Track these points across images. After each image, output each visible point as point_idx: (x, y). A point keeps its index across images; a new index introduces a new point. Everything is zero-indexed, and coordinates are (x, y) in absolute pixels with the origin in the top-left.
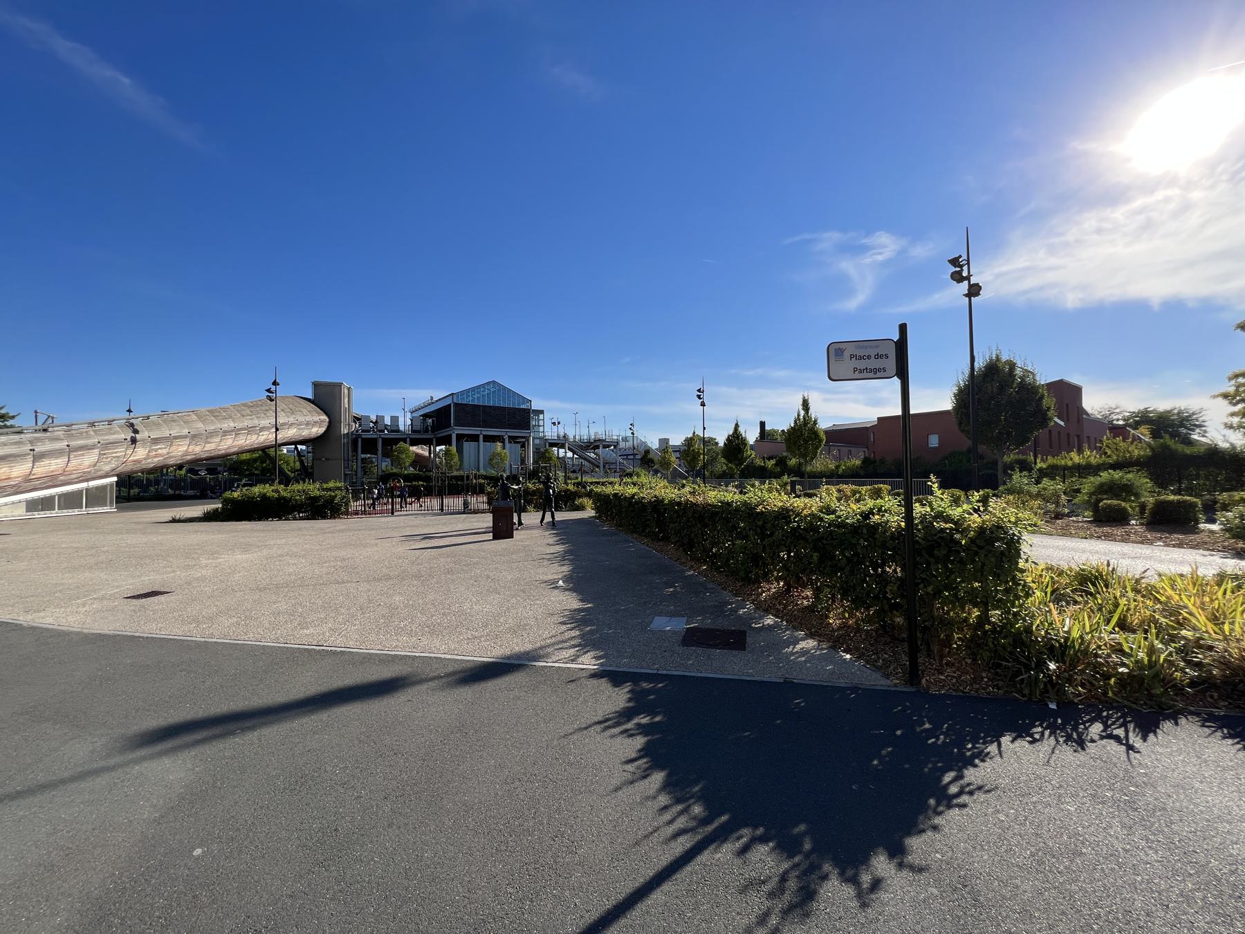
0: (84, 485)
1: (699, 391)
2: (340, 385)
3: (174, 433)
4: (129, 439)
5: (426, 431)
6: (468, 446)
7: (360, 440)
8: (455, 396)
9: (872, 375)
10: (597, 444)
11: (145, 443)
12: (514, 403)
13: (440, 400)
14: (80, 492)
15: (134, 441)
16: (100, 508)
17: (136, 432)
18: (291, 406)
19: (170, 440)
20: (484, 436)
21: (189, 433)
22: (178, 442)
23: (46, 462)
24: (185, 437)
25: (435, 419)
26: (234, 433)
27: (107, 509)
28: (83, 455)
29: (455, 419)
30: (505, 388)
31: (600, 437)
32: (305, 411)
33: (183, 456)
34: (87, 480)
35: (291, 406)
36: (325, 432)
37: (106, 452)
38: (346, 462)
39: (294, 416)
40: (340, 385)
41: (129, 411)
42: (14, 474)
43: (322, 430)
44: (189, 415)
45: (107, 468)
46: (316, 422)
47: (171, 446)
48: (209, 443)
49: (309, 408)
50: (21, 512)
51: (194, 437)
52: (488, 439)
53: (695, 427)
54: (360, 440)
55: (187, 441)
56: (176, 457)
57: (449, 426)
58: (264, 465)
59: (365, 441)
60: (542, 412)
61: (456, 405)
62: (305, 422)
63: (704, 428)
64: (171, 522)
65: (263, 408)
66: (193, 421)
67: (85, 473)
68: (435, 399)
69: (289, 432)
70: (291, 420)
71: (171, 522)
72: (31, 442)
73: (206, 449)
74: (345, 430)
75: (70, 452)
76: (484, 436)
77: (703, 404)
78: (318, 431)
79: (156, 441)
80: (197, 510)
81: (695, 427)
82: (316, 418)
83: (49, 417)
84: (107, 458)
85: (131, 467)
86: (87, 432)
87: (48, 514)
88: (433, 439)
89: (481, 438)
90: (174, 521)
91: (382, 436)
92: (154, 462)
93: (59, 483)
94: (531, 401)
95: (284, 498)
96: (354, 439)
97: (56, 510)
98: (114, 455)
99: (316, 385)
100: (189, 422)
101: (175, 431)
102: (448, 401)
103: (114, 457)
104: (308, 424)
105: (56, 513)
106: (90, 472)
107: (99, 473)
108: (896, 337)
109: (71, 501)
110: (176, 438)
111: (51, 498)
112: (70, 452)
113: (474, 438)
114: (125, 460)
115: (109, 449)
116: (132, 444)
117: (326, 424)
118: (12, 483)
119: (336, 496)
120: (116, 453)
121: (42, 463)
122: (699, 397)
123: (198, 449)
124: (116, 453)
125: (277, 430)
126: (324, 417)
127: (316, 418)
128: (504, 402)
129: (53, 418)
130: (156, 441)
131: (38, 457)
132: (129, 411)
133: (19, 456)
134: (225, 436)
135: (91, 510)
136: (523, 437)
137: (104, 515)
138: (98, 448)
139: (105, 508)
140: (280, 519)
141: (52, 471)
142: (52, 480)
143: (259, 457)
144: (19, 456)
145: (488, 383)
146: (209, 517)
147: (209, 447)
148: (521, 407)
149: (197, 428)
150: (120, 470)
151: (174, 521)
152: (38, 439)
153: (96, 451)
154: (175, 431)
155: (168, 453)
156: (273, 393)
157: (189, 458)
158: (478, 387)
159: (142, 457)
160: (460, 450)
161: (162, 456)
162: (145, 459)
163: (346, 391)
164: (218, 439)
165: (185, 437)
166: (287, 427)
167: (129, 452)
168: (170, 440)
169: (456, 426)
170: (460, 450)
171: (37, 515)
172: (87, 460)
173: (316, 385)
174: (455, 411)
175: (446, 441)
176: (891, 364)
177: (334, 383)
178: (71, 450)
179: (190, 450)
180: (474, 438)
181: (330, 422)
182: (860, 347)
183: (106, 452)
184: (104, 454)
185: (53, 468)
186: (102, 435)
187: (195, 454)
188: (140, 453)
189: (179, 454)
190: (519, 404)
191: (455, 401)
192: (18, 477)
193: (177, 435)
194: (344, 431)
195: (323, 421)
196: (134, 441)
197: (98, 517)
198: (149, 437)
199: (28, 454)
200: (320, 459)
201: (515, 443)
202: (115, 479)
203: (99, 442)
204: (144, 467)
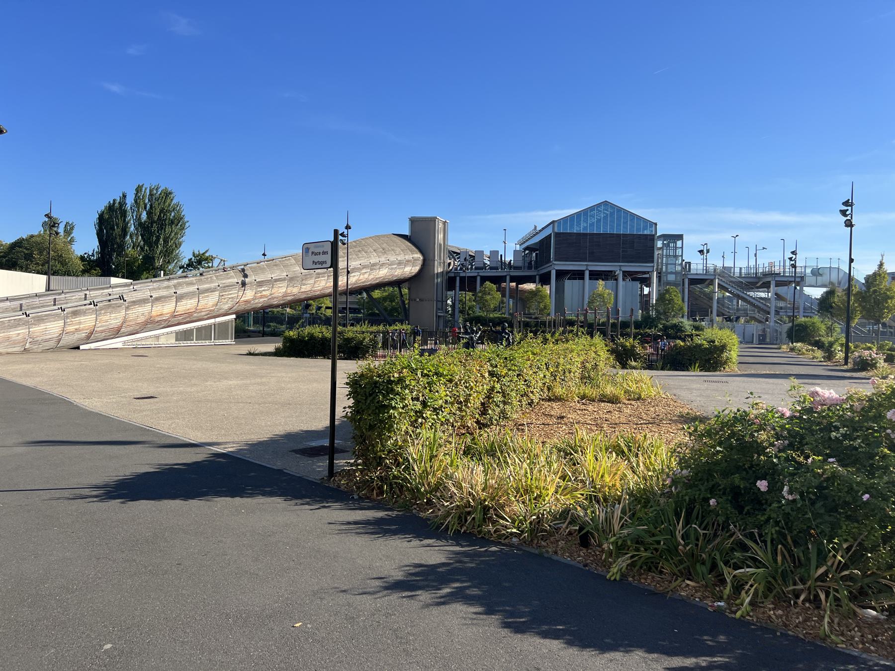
0: (212, 321)
1: (846, 203)
2: (433, 220)
3: (275, 276)
4: (240, 283)
5: (530, 267)
6: (570, 285)
7: (458, 279)
8: (556, 224)
9: (320, 266)
10: (768, 279)
11: (252, 286)
12: (638, 229)
13: (543, 229)
14: (210, 326)
15: (244, 284)
16: (224, 341)
17: (246, 276)
18: (385, 245)
19: (272, 282)
20: (590, 271)
21: (287, 276)
22: (279, 284)
23: (184, 302)
24: (284, 280)
25: (538, 252)
26: (326, 275)
27: (228, 342)
28: (208, 296)
29: (555, 253)
30: (620, 209)
31: (777, 270)
32: (398, 250)
33: (283, 296)
34: (215, 317)
35: (385, 245)
36: (420, 271)
37: (224, 293)
38: (440, 304)
39: (385, 256)
40: (433, 220)
41: (264, 255)
42: (165, 311)
43: (416, 269)
44: (289, 259)
45: (226, 307)
46: (408, 261)
47: (272, 287)
48: (305, 284)
49: (403, 247)
50: (172, 341)
51: (291, 280)
52: (596, 275)
53: (882, 256)
54: (458, 279)
55: (285, 284)
56: (277, 298)
57: (549, 261)
58: (394, 304)
59: (462, 279)
60: (680, 237)
61: (558, 235)
62: (397, 262)
63: (851, 261)
64: (247, 354)
65: (356, 250)
66: (291, 265)
67: (211, 311)
68: (539, 228)
69: (381, 272)
70: (383, 259)
71: (247, 354)
72: (175, 286)
73: (302, 290)
74: (439, 269)
75: (199, 294)
76: (590, 271)
77: (849, 224)
78: (411, 270)
79: (260, 284)
80: (271, 348)
81: (882, 256)
82: (409, 257)
83: (221, 260)
84: (225, 299)
85: (243, 306)
86: (211, 277)
87: (189, 343)
88: (535, 276)
89: (508, 278)
90: (250, 354)
91: (481, 274)
92: (260, 302)
93: (195, 319)
94: (656, 224)
95: (326, 338)
96: (450, 281)
97: (195, 341)
98: (229, 296)
99: (413, 221)
100: (288, 265)
101: (276, 275)
102: (549, 231)
103: (230, 298)
104: (400, 263)
105: (194, 342)
106: (214, 310)
107: (221, 311)
108: (332, 239)
109: (204, 333)
110: (276, 280)
111: (191, 331)
112: (199, 294)
113: (579, 275)
114: (238, 300)
115: (226, 292)
116: (242, 287)
117: (420, 263)
118: (164, 318)
119: (364, 339)
120: (231, 294)
121: (181, 303)
122: (844, 213)
123: (295, 290)
124: (231, 294)
125: (348, 272)
126: (419, 256)
127: (409, 257)
128: (612, 227)
129: (224, 261)
130: (260, 284)
131: (179, 298)
132: (264, 255)
133: (167, 297)
134: (319, 278)
135: (218, 342)
136: (644, 273)
137: (223, 346)
138: (218, 290)
139: (227, 341)
140: (324, 358)
141: (189, 310)
142: (189, 318)
143: (388, 295)
144: (167, 297)
145: (599, 205)
146: (278, 353)
147: (305, 288)
148: (646, 232)
149: (294, 271)
150: (236, 308)
151: (250, 354)
152: (179, 284)
153: (217, 293)
154: (276, 275)
155: (271, 294)
156: (345, 237)
157: (289, 298)
158: (591, 209)
159: (252, 297)
160: (560, 291)
161: (266, 297)
162: (253, 299)
163: (441, 225)
164: (312, 281)
165: (284, 280)
166: (378, 267)
167: (241, 293)
168: (272, 282)
169: (555, 260)
170: (560, 291)
171: (182, 343)
172: (209, 301)
173: (413, 221)
174: (556, 243)
175: (545, 279)
176: (328, 258)
177: (428, 218)
178: (200, 292)
179: (289, 291)
180: (579, 275)
181: (424, 261)
182: (316, 247)
183: (224, 293)
184: (223, 295)
185: (188, 307)
186: (221, 279)
187: (294, 295)
188: (249, 294)
189: (280, 295)
190: (638, 229)
191: (556, 230)
192: (168, 314)
193: (277, 278)
194: (437, 270)
195: (415, 260)
196: (244, 284)
197: (109, 336)
198: (255, 280)
199: (173, 296)
200: (415, 300)
201: (634, 279)
202: (234, 316)
203: (219, 286)
204: (254, 306)
